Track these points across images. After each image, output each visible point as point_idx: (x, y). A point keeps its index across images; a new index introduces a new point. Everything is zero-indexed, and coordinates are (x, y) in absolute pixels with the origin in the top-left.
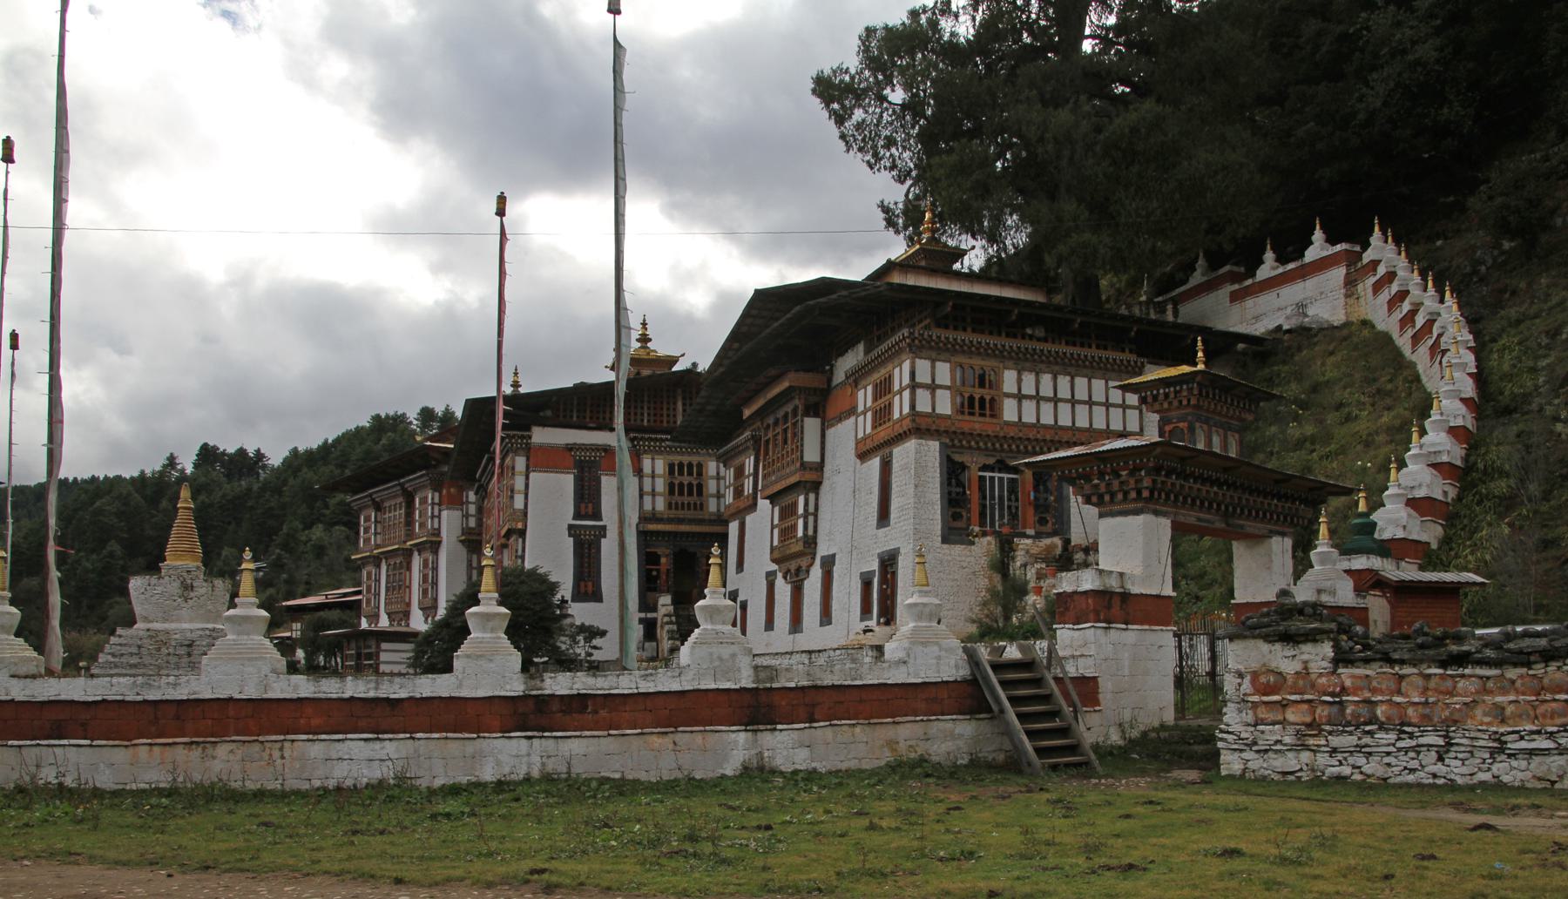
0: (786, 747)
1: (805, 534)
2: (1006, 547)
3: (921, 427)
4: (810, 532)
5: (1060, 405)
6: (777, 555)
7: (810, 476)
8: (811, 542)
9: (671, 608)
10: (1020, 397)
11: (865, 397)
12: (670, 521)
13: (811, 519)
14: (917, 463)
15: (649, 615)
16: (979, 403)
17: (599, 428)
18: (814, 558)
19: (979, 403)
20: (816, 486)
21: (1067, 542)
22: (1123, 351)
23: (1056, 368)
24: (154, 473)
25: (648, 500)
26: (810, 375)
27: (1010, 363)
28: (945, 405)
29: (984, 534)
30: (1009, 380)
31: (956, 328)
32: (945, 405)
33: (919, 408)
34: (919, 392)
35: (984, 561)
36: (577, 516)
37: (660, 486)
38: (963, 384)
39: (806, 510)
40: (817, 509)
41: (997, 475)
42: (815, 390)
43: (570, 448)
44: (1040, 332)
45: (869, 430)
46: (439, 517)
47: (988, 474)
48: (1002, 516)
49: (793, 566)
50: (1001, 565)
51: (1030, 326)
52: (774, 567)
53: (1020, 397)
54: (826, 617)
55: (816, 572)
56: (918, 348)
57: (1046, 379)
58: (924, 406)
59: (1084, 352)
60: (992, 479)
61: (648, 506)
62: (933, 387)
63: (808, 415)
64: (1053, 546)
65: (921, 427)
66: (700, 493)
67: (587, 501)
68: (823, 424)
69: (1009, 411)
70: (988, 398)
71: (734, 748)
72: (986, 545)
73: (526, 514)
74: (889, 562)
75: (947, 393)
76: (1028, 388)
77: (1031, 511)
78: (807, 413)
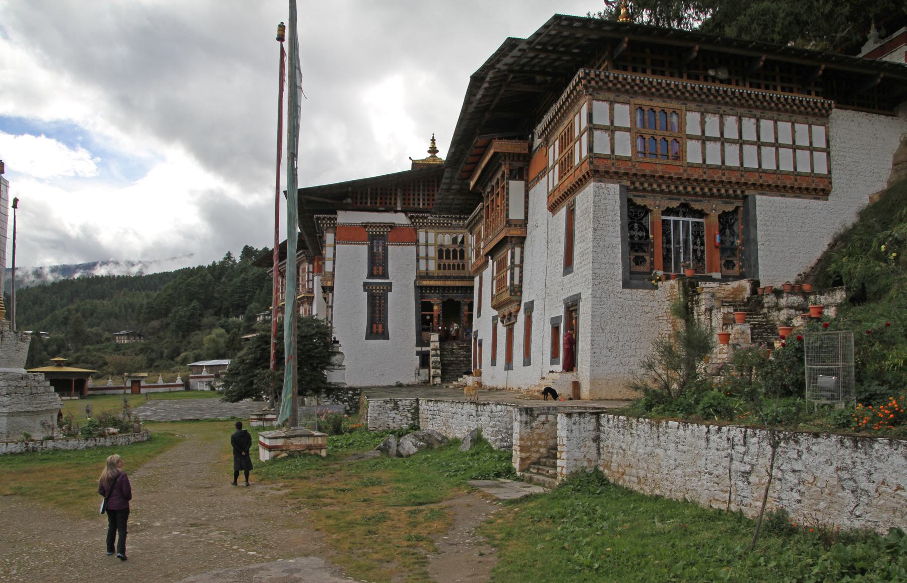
1: (512, 284)
2: (690, 289)
3: (600, 170)
4: (516, 282)
6: (495, 303)
7: (515, 232)
8: (517, 290)
9: (438, 344)
10: (704, 139)
11: (554, 153)
12: (439, 278)
13: (517, 270)
14: (599, 204)
15: (424, 349)
16: (659, 139)
18: (520, 305)
19: (659, 139)
20: (521, 241)
21: (756, 284)
22: (809, 93)
23: (740, 111)
24: (220, 262)
25: (423, 263)
26: (513, 142)
27: (693, 106)
28: (624, 147)
29: (668, 278)
30: (692, 121)
31: (635, 70)
32: (624, 147)
33: (596, 150)
34: (597, 133)
35: (667, 305)
36: (371, 275)
37: (432, 252)
38: (644, 126)
39: (512, 263)
40: (522, 261)
41: (681, 219)
42: (519, 155)
43: (365, 225)
44: (723, 74)
45: (556, 182)
46: (313, 280)
47: (672, 218)
48: (687, 258)
49: (506, 311)
50: (686, 312)
51: (712, 68)
52: (495, 313)
53: (704, 139)
54: (527, 362)
55: (521, 317)
56: (597, 90)
57: (731, 121)
58: (602, 146)
60: (676, 223)
61: (423, 268)
62: (611, 129)
63: (514, 179)
64: (741, 289)
65: (600, 170)
66: (462, 257)
67: (377, 265)
68: (526, 186)
72: (669, 290)
73: (333, 276)
74: (572, 307)
76: (712, 130)
77: (717, 254)
78: (512, 177)
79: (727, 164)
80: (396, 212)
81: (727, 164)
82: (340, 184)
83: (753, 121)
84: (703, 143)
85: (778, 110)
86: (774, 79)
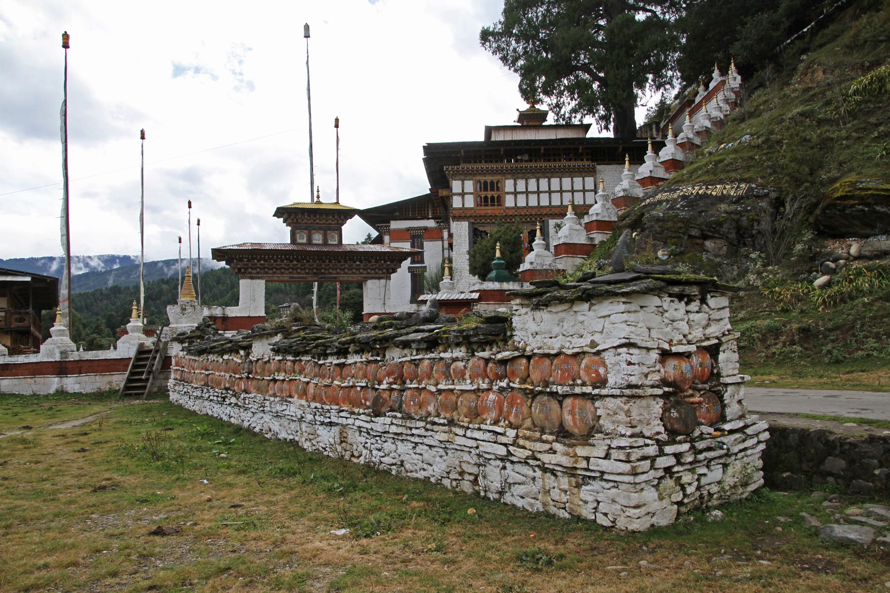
0: (72, 383)
5: (553, 195)
10: (516, 193)
17: (422, 219)
23: (538, 175)
27: (509, 176)
30: (509, 185)
43: (408, 229)
44: (526, 157)
59: (557, 164)
69: (509, 202)
70: (496, 196)
71: (53, 383)
75: (472, 196)
79: (541, 204)
80: (428, 219)
81: (541, 204)
82: (376, 208)
83: (547, 179)
84: (516, 196)
85: (561, 173)
86: (559, 155)
